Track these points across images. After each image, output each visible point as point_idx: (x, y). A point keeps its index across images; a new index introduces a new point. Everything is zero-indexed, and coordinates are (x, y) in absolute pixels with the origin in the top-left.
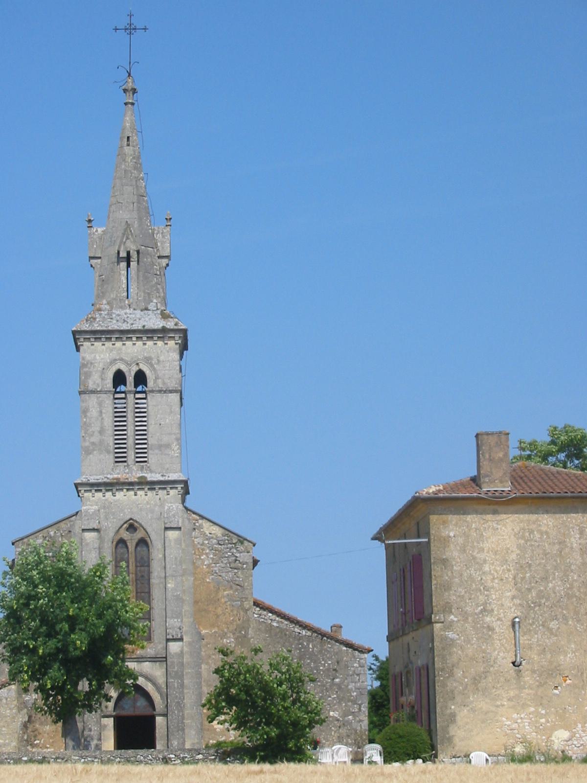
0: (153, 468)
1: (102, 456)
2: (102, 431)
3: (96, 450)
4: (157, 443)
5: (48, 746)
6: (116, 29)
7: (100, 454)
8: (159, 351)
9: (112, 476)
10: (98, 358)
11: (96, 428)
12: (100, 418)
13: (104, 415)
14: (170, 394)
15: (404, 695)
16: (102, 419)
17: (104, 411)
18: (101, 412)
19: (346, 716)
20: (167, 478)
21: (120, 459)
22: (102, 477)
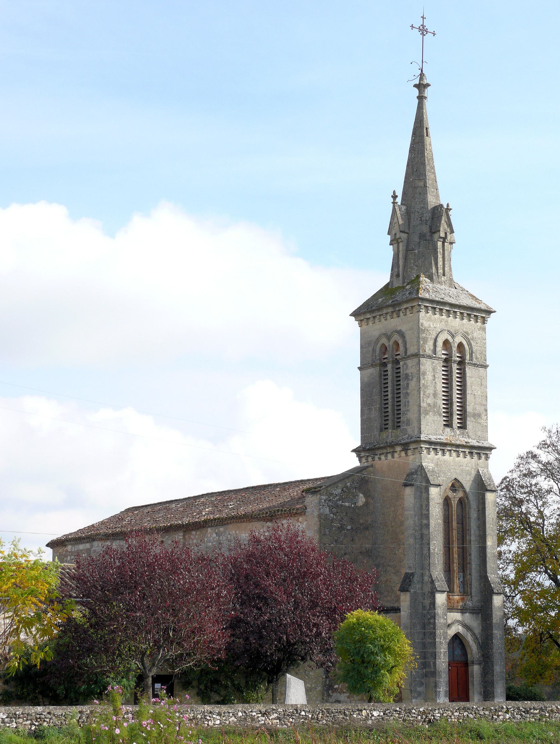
0: (470, 434)
1: (435, 417)
2: (435, 395)
3: (431, 411)
4: (472, 411)
5: (345, 691)
6: (423, 18)
7: (434, 415)
8: (473, 328)
9: (443, 438)
10: (432, 326)
11: (430, 391)
12: (434, 382)
13: (436, 380)
14: (481, 369)
15: (396, 605)
16: (435, 383)
17: (436, 376)
18: (434, 376)
19: (137, 712)
20: (480, 445)
21: (448, 424)
22: (435, 437)
